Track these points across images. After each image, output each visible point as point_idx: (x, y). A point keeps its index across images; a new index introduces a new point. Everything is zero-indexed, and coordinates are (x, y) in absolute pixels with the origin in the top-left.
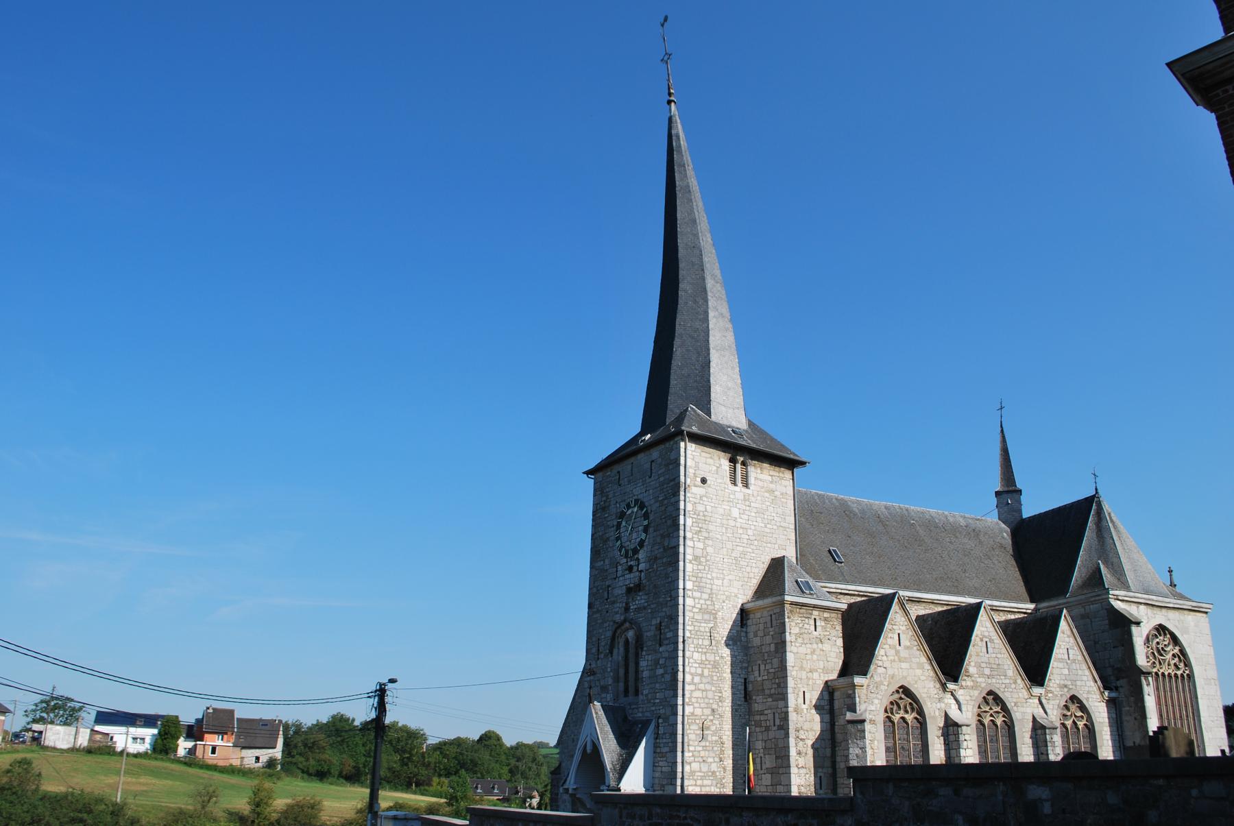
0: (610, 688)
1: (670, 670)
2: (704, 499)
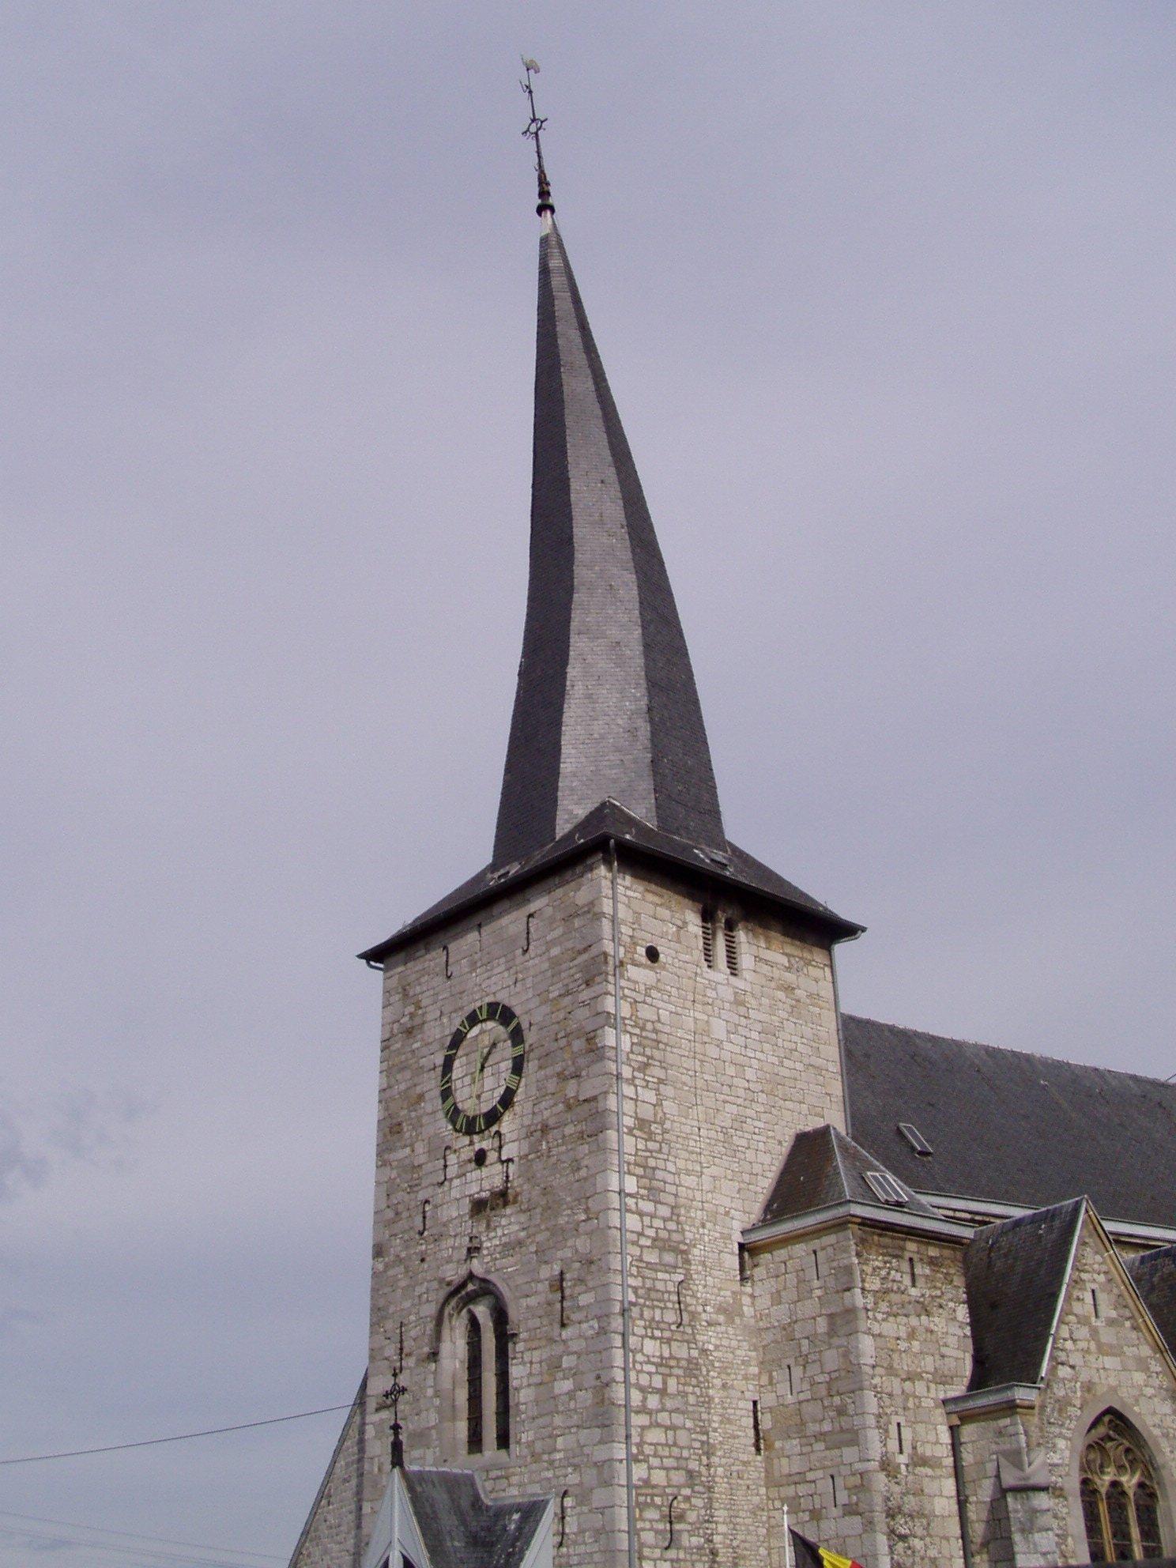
1: (589, 1380)
2: (654, 993)
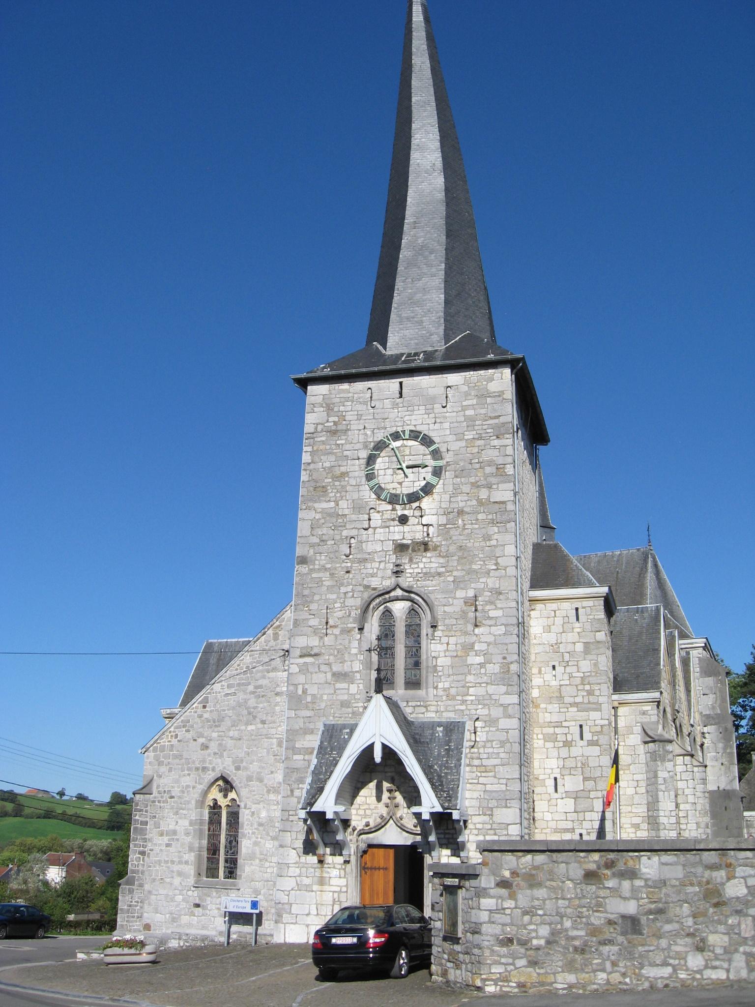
0: (358, 676)
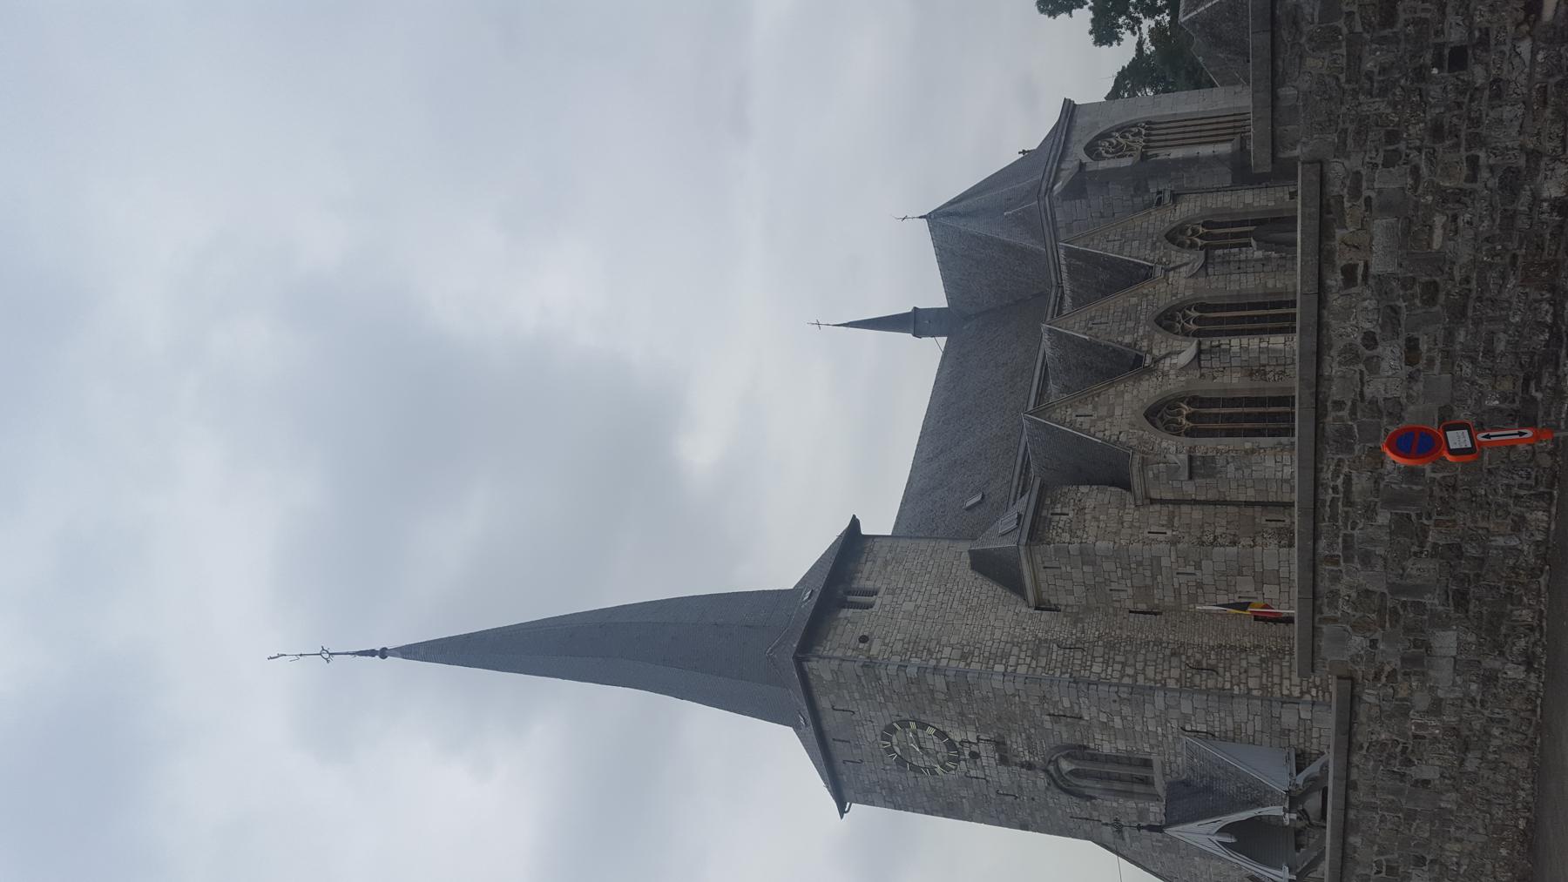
2: (887, 641)
